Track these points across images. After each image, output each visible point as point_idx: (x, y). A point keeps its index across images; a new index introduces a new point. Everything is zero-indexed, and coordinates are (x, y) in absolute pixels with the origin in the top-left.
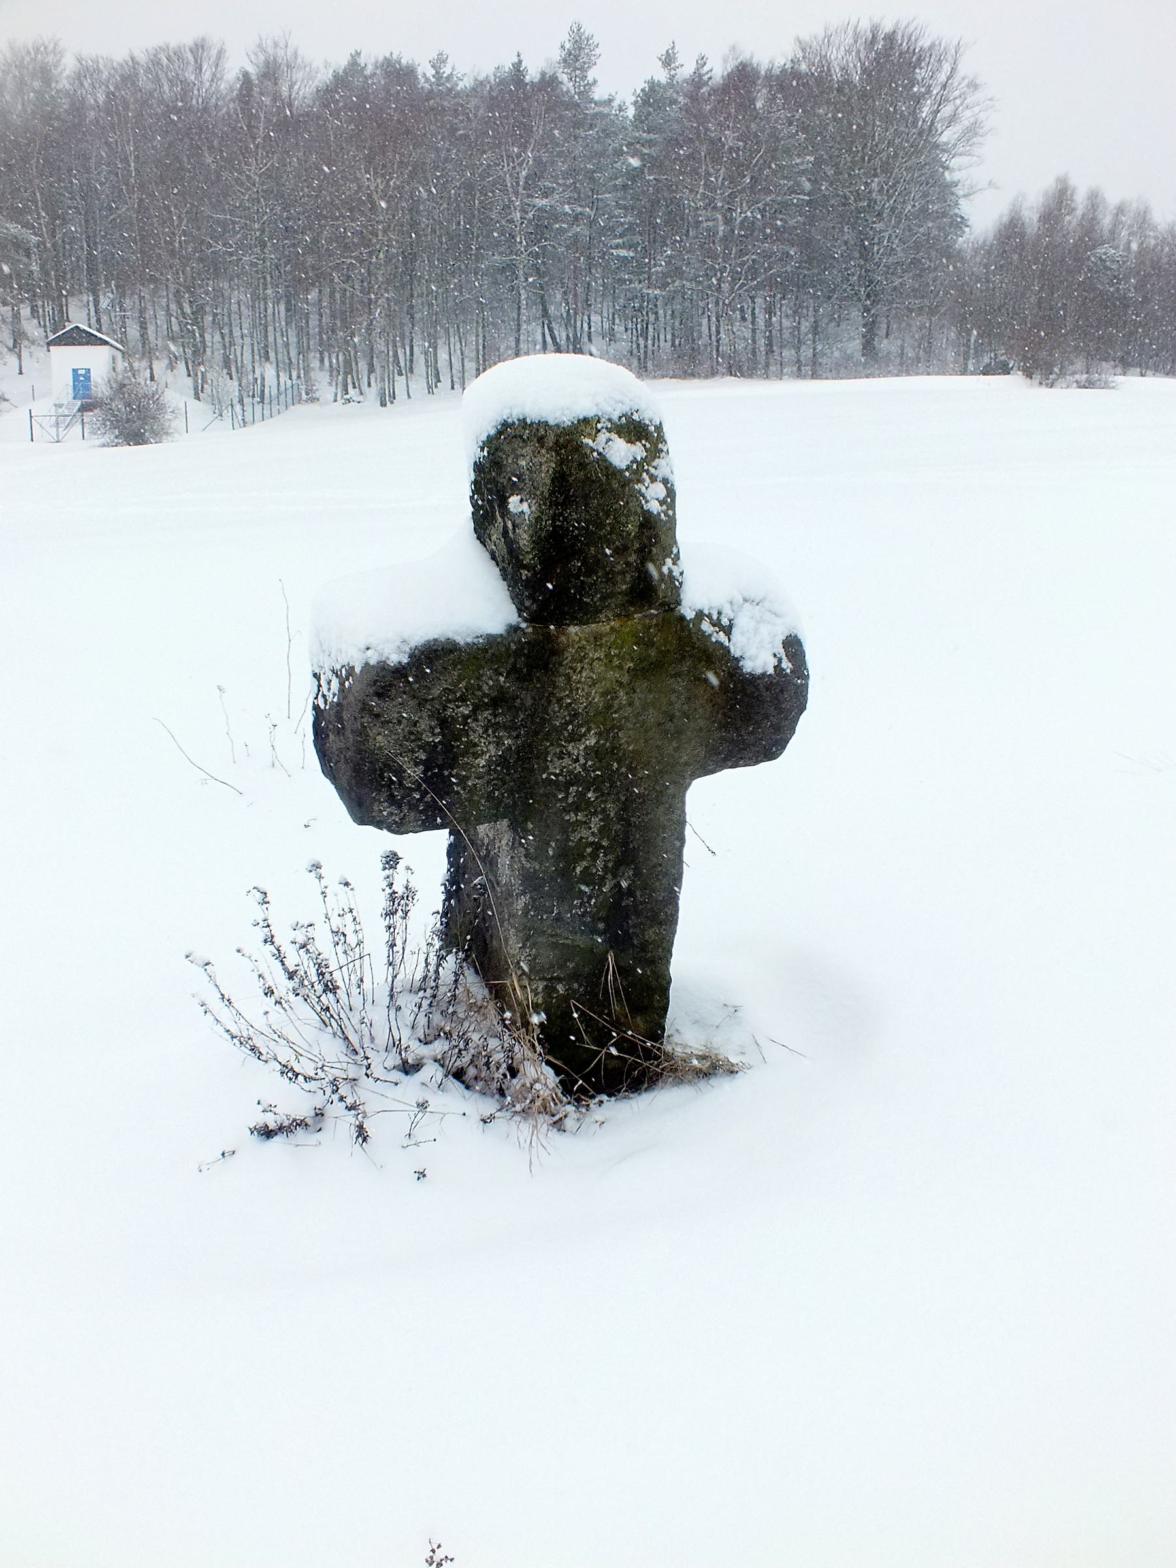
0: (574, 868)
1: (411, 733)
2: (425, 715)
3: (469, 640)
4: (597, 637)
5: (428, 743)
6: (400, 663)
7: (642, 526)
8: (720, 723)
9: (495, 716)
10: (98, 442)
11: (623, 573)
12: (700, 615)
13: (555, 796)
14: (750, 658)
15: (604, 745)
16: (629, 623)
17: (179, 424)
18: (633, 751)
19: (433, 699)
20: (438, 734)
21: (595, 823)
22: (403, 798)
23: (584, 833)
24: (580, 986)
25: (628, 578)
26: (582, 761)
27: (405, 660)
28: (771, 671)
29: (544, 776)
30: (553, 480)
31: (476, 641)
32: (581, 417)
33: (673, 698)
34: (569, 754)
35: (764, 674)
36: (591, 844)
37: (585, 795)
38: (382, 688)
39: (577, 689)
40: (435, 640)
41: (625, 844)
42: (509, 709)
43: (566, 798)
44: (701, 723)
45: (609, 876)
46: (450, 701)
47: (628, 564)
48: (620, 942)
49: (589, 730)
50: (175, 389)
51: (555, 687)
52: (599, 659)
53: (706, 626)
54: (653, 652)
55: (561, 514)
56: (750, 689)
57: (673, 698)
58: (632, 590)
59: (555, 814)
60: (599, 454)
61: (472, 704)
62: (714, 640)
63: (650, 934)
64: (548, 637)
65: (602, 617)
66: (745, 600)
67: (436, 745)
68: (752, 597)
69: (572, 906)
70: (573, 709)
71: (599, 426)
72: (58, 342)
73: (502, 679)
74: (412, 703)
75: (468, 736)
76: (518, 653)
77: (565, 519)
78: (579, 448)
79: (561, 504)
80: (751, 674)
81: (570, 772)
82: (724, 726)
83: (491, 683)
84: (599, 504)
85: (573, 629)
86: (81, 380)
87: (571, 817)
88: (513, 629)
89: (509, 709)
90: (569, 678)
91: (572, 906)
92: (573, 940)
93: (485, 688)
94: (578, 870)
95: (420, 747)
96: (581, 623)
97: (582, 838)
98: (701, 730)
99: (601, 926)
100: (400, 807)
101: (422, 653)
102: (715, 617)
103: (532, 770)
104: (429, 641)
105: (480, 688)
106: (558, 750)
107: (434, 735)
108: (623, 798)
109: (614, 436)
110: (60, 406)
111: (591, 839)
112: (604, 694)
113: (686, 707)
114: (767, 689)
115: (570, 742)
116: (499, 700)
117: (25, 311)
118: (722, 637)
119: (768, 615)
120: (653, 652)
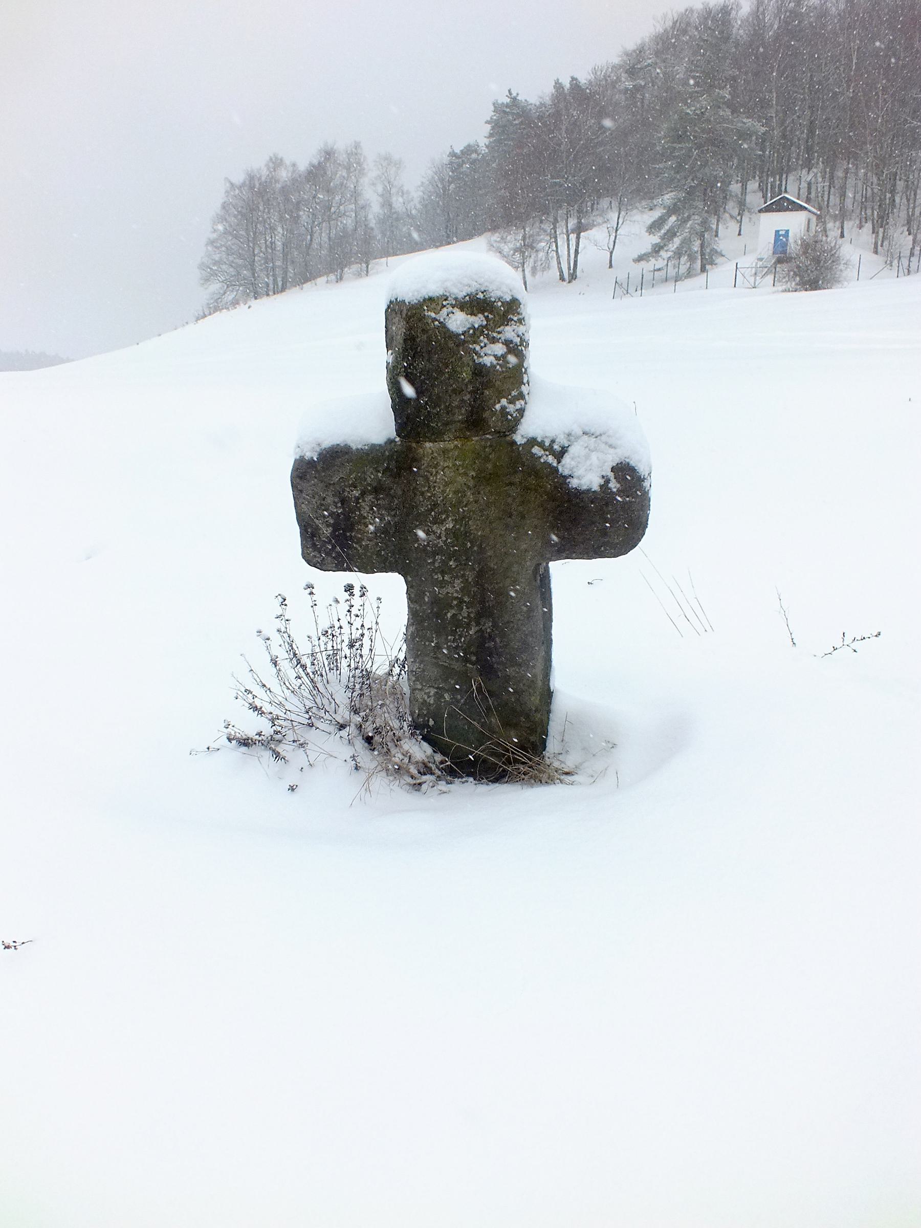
0: (446, 614)
1: (322, 505)
2: (330, 493)
3: (359, 447)
4: (445, 451)
5: (334, 513)
10: (780, 288)
11: (459, 407)
12: (532, 442)
13: (426, 561)
14: (578, 478)
15: (459, 529)
17: (851, 273)
18: (481, 536)
21: (458, 584)
22: (321, 547)
24: (462, 698)
25: (463, 411)
26: (444, 539)
28: (595, 487)
30: (405, 340)
33: (510, 500)
34: (435, 533)
35: (589, 490)
41: (482, 602)
42: (387, 495)
43: (433, 563)
45: (473, 623)
46: (346, 486)
49: (448, 517)
50: (854, 247)
52: (448, 467)
53: (536, 450)
54: (489, 466)
57: (510, 500)
62: (542, 460)
64: (410, 449)
67: (338, 515)
68: (592, 431)
69: (447, 641)
71: (444, 303)
72: (768, 209)
73: (380, 475)
74: (321, 485)
76: (390, 458)
78: (422, 318)
85: (428, 445)
86: (781, 239)
88: (390, 441)
90: (427, 479)
91: (447, 641)
93: (369, 480)
94: (449, 615)
99: (474, 658)
102: (547, 444)
103: (406, 540)
105: (366, 480)
107: (337, 507)
109: (456, 310)
110: (761, 259)
111: (456, 595)
112: (455, 492)
113: (521, 509)
116: (377, 490)
117: (753, 185)
118: (551, 459)
119: (603, 446)
120: (489, 466)
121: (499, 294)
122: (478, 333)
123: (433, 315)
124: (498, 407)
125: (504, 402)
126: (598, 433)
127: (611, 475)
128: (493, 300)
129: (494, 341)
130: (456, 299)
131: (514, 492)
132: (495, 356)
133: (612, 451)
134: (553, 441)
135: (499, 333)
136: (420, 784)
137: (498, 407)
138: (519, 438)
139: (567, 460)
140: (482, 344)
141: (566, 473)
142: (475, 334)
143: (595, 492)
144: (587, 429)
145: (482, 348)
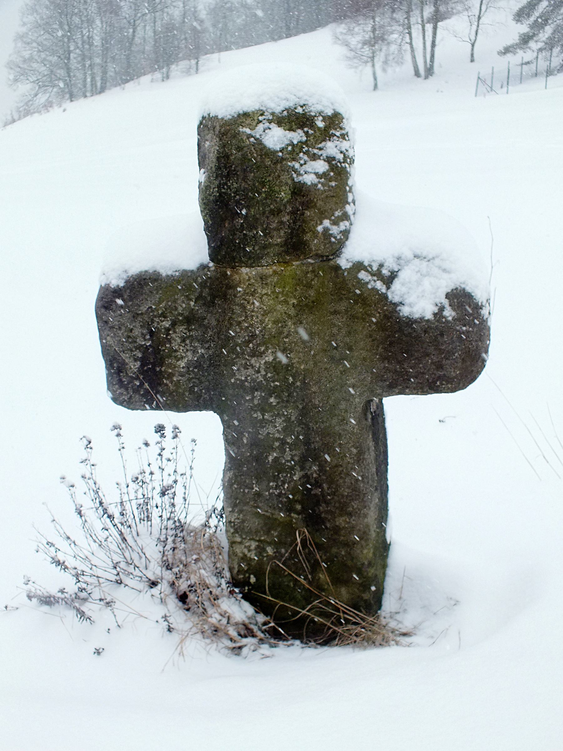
0: (267, 457)
2: (138, 324)
3: (170, 273)
4: (262, 278)
5: (142, 346)
6: (118, 286)
7: (294, 193)
8: (381, 355)
9: (189, 331)
12: (359, 266)
16: (289, 268)
18: (304, 370)
19: (142, 314)
20: (149, 340)
21: (280, 423)
22: (128, 384)
23: (271, 430)
25: (282, 233)
26: (263, 373)
27: (122, 284)
28: (429, 316)
29: (233, 381)
31: (174, 274)
32: (241, 112)
34: (252, 366)
35: (422, 319)
36: (278, 439)
37: (268, 399)
38: (107, 302)
39: (252, 316)
40: (146, 271)
42: (200, 326)
44: (364, 354)
46: (155, 317)
47: (281, 222)
48: (314, 521)
49: (267, 349)
51: (233, 313)
52: (266, 294)
53: (363, 275)
54: (312, 293)
55: (226, 184)
56: (407, 330)
58: (286, 243)
59: (245, 411)
60: (256, 139)
61: (171, 319)
63: (341, 521)
65: (263, 262)
66: (416, 256)
70: (251, 332)
73: (192, 303)
75: (170, 343)
76: (203, 285)
77: (229, 187)
78: (236, 135)
79: (225, 176)
80: (407, 317)
81: (254, 380)
82: (384, 358)
83: (184, 305)
84: (254, 177)
87: (259, 415)
88: (203, 267)
89: (200, 326)
90: (244, 307)
91: (268, 488)
92: (272, 514)
94: (270, 458)
95: (136, 348)
96: (251, 266)
97: (269, 433)
98: (364, 359)
100: (127, 389)
101: (135, 280)
104: (141, 272)
105: (176, 309)
106: (244, 362)
108: (300, 407)
109: (273, 126)
111: (277, 435)
113: (347, 340)
114: (426, 332)
115: (253, 356)
116: (190, 319)
118: (379, 285)
119: (436, 271)
120: (312, 293)
121: (319, 108)
122: (297, 150)
123: (248, 131)
124: (320, 228)
125: (327, 223)
126: (430, 256)
127: (446, 302)
128: (313, 114)
129: (314, 157)
130: (273, 114)
131: (339, 321)
132: (316, 174)
133: (445, 276)
134: (381, 266)
135: (320, 149)
136: (240, 648)
137: (320, 228)
138: (344, 262)
139: (396, 285)
140: (302, 162)
141: (396, 299)
142: (294, 151)
143: (428, 321)
144: (418, 252)
145: (301, 165)
